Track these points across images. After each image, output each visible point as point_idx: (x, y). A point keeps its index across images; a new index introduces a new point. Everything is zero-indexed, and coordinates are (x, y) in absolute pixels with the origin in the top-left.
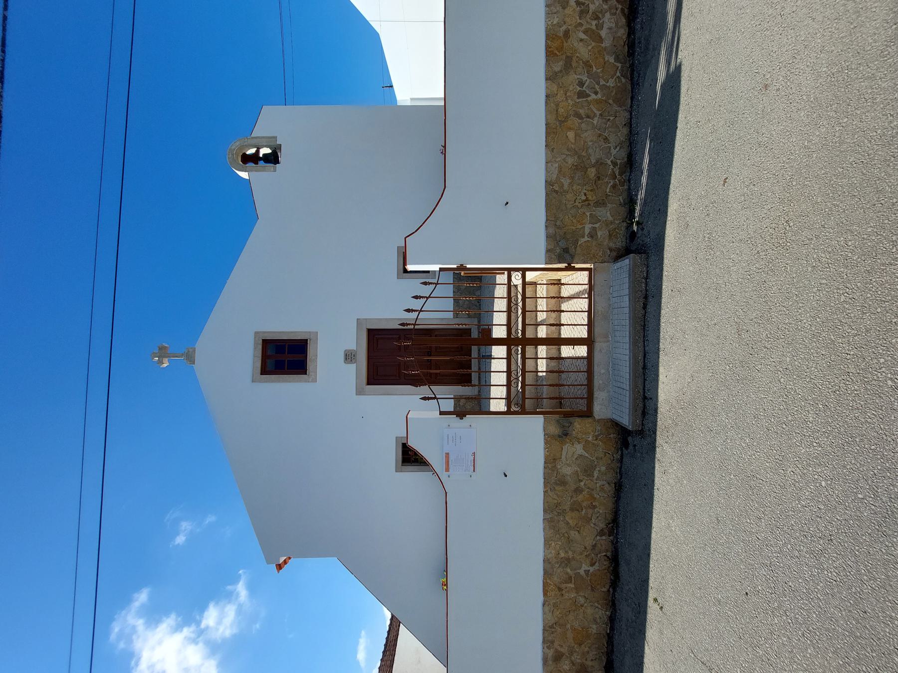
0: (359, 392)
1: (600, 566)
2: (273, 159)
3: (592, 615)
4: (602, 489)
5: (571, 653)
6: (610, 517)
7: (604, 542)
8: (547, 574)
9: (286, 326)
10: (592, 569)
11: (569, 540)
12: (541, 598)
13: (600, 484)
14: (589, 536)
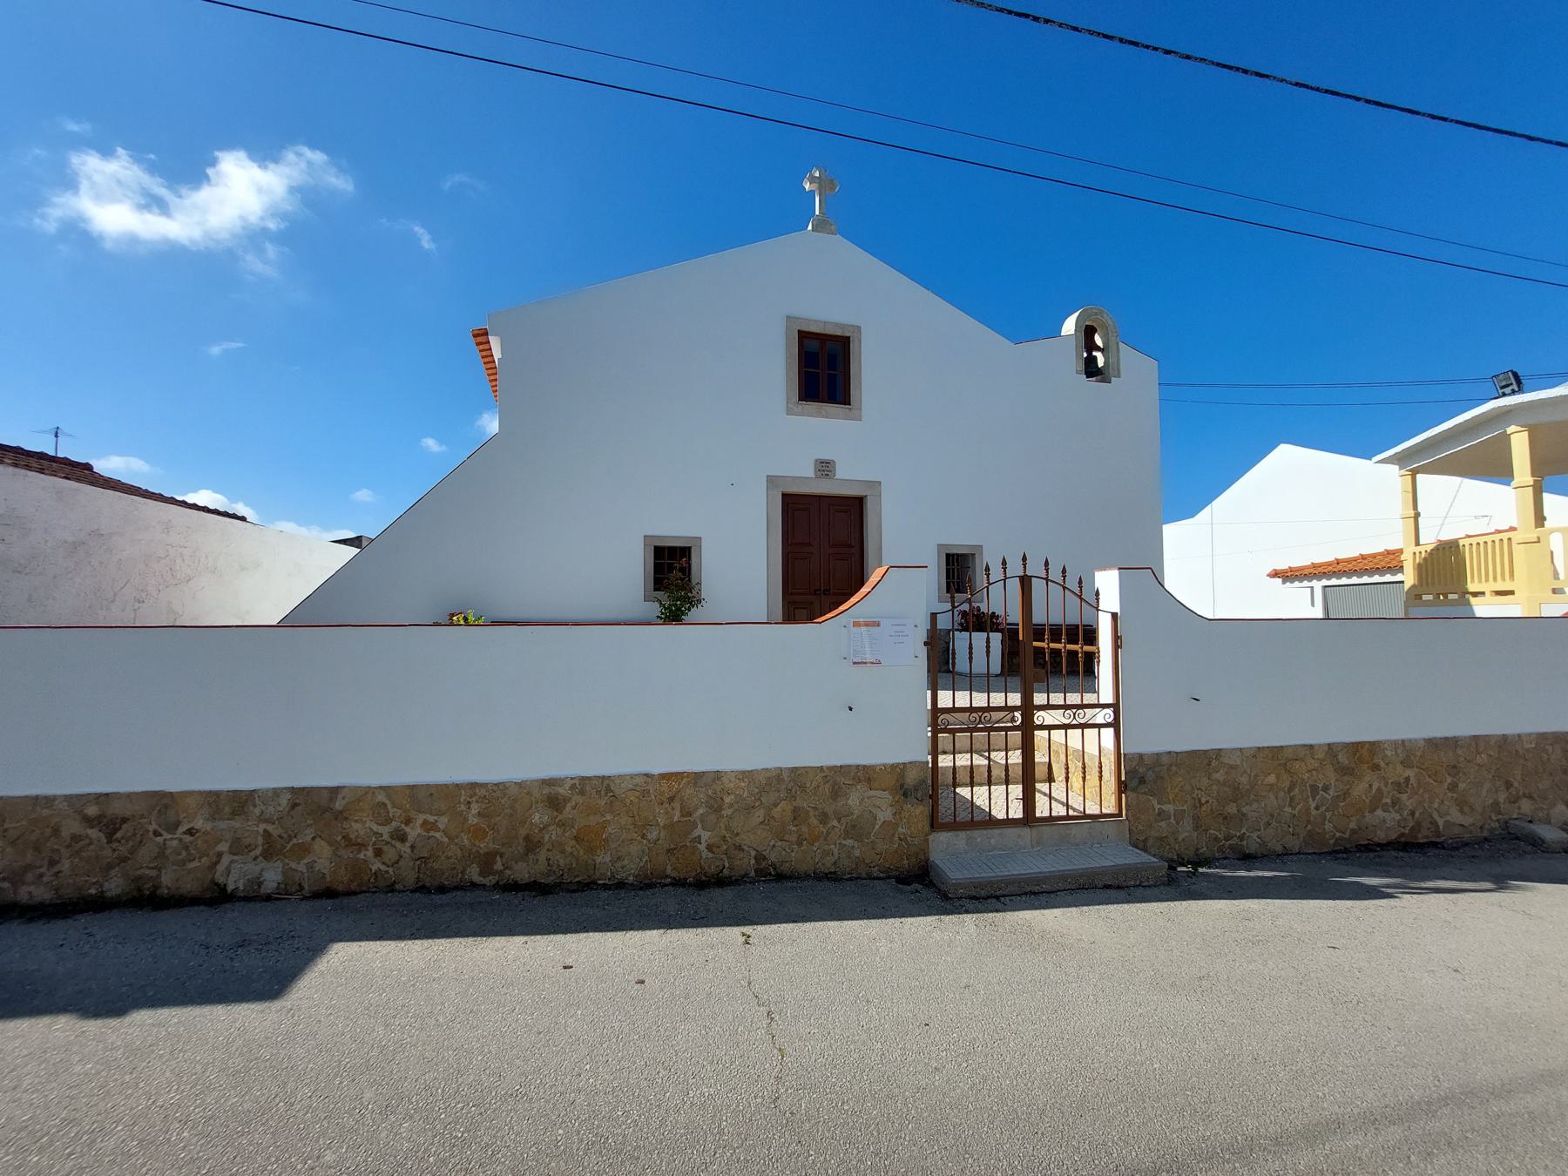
0: (771, 480)
1: (707, 860)
2: (1091, 369)
3: (627, 853)
4: (829, 853)
5: (562, 824)
6: (785, 868)
7: (747, 863)
9: (871, 370)
10: (702, 847)
11: (749, 809)
12: (656, 770)
14: (756, 838)
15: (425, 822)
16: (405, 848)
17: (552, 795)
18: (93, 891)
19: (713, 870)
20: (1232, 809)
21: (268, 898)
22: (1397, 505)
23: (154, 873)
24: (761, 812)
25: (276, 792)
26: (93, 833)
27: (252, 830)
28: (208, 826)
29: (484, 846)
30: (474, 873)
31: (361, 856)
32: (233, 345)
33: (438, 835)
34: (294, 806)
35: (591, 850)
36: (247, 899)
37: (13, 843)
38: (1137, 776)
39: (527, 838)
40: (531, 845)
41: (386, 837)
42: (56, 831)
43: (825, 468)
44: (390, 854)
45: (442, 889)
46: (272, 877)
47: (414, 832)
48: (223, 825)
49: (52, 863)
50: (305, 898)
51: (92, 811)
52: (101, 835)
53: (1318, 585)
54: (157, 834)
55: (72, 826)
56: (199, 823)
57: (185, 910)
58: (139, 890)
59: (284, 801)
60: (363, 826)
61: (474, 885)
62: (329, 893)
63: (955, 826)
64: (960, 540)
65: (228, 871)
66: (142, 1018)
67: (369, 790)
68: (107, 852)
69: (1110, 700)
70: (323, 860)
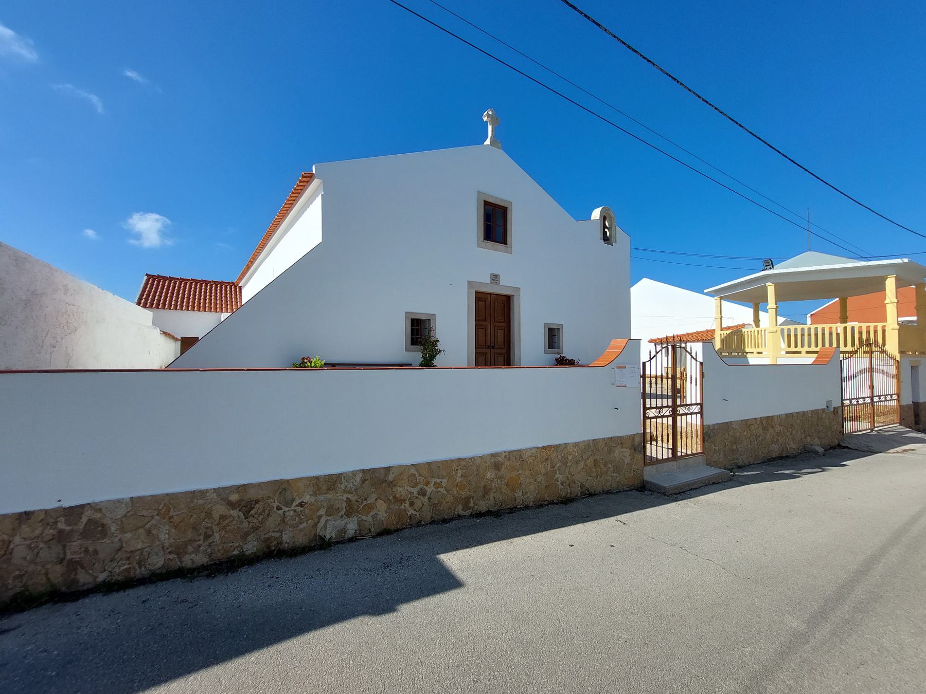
0: (470, 284)
1: (564, 491)
2: (606, 239)
3: (529, 491)
4: (607, 481)
5: (500, 478)
6: (592, 491)
7: (577, 490)
8: (557, 447)
9: (518, 225)
10: (559, 483)
11: (577, 462)
12: (540, 445)
13: (611, 479)
14: (581, 477)
15: (435, 483)
16: (425, 500)
17: (496, 462)
18: (236, 552)
19: (564, 494)
20: (734, 447)
21: (352, 540)
22: (714, 312)
23: (277, 535)
24: (582, 463)
25: (354, 473)
26: (234, 513)
27: (340, 498)
28: (313, 499)
29: (465, 493)
30: (460, 510)
31: (403, 507)
32: (899, 261)
33: (442, 490)
34: (364, 481)
35: (513, 490)
36: (338, 543)
37: (176, 527)
38: (708, 434)
39: (485, 487)
40: (486, 491)
41: (415, 494)
42: (209, 514)
43: (495, 278)
44: (418, 504)
45: (445, 521)
46: (352, 527)
47: (430, 489)
48: (322, 498)
49: (207, 537)
50: (373, 537)
51: (234, 497)
52: (241, 514)
54: (279, 508)
55: (220, 510)
56: (307, 498)
57: (299, 559)
58: (268, 547)
59: (358, 478)
60: (401, 490)
61: (459, 516)
62: (385, 532)
63: (649, 464)
64: (554, 321)
65: (325, 526)
66: (406, 609)
67: (407, 467)
68: (246, 524)
69: (698, 402)
70: (382, 512)
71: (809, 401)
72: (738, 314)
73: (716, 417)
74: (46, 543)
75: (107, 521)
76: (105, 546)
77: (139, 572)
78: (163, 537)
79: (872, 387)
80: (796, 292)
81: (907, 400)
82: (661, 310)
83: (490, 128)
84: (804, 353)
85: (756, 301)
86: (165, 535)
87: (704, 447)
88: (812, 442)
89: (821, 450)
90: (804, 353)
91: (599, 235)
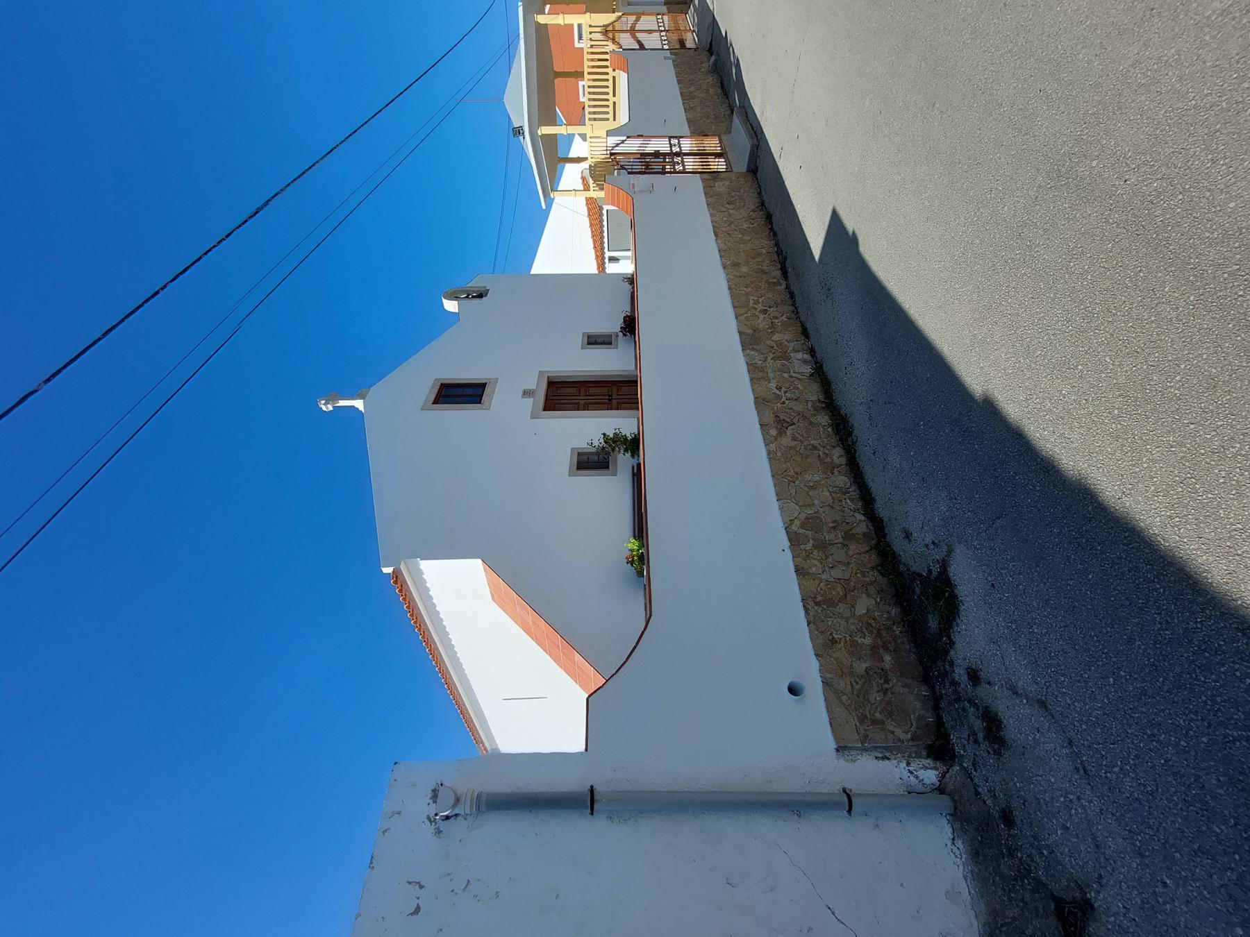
0: (533, 416)
2: (480, 296)
3: (763, 244)
23: (810, 404)
32: (521, 9)
43: (527, 393)
48: (771, 375)
51: (774, 432)
53: (608, 254)
56: (773, 385)
60: (762, 323)
64: (579, 340)
70: (786, 337)
71: (666, 73)
72: (571, 176)
73: (680, 121)
74: (827, 557)
75: (803, 516)
76: (828, 517)
77: (854, 492)
78: (816, 478)
79: (650, 32)
80: (545, 111)
81: (664, 9)
82: (566, 243)
83: (342, 403)
84: (615, 99)
85: (554, 156)
86: (814, 477)
87: (714, 135)
88: (711, 77)
89: (713, 58)
90: (615, 99)
91: (478, 301)
